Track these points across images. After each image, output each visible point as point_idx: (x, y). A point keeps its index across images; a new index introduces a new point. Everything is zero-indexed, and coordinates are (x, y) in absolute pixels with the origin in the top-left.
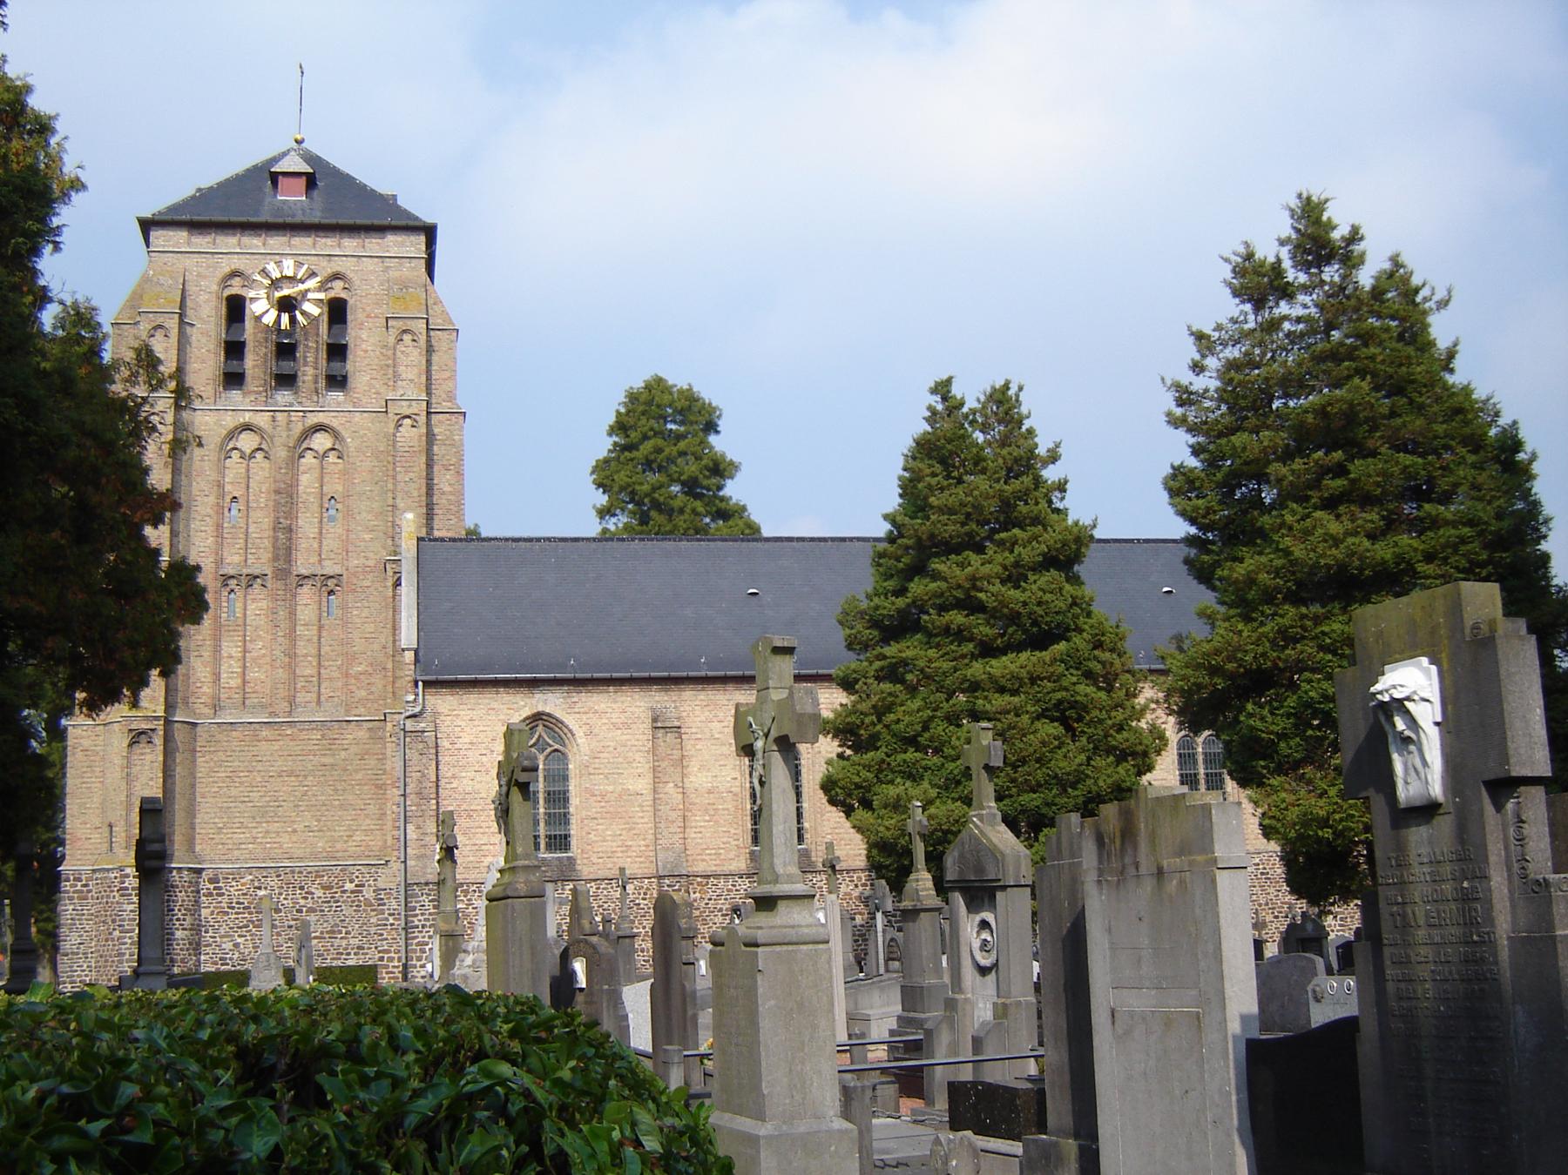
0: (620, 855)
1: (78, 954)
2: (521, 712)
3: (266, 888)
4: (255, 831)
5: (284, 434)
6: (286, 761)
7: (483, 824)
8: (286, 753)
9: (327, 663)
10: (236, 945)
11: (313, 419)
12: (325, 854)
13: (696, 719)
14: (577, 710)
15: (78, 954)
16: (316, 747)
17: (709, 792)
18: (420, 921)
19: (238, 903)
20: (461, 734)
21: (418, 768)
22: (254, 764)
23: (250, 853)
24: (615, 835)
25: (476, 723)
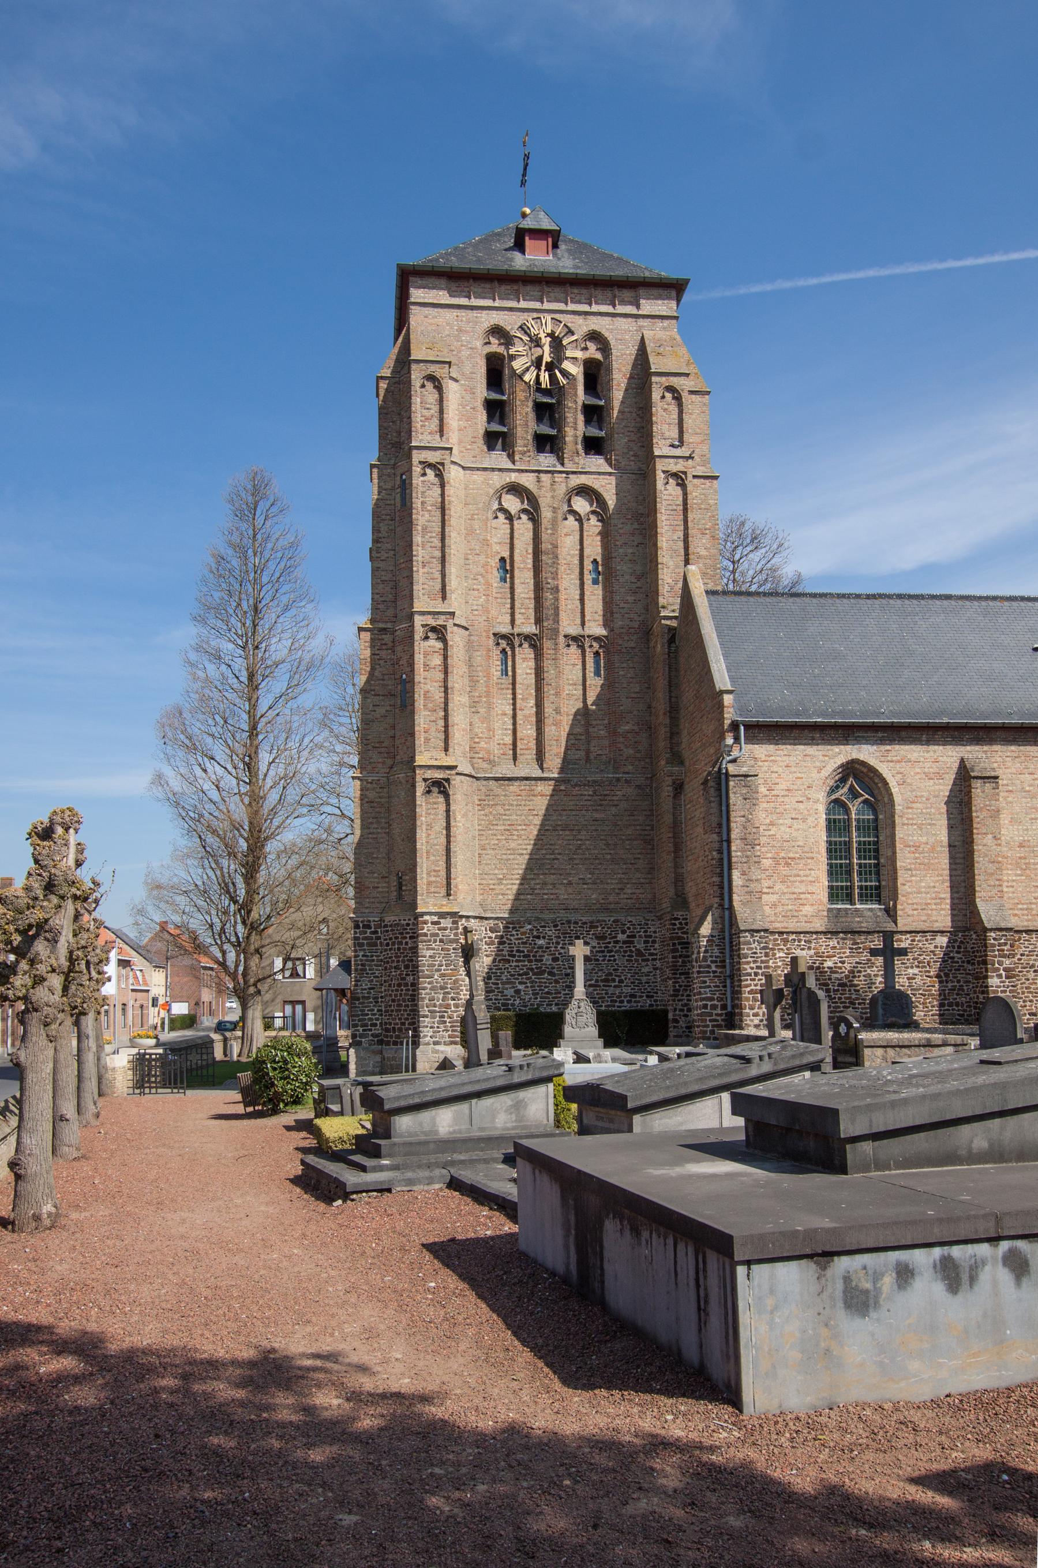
0: (934, 907)
1: (368, 998)
2: (836, 760)
3: (544, 938)
4: (533, 882)
5: (549, 495)
6: (561, 815)
7: (801, 873)
8: (560, 808)
9: (594, 723)
10: (518, 992)
11: (576, 481)
12: (598, 906)
13: (1007, 771)
14: (889, 758)
15: (368, 998)
16: (589, 803)
17: (1021, 846)
18: (752, 968)
19: (518, 951)
20: (777, 781)
21: (742, 813)
22: (531, 818)
23: (529, 903)
24: (929, 887)
25: (793, 769)
